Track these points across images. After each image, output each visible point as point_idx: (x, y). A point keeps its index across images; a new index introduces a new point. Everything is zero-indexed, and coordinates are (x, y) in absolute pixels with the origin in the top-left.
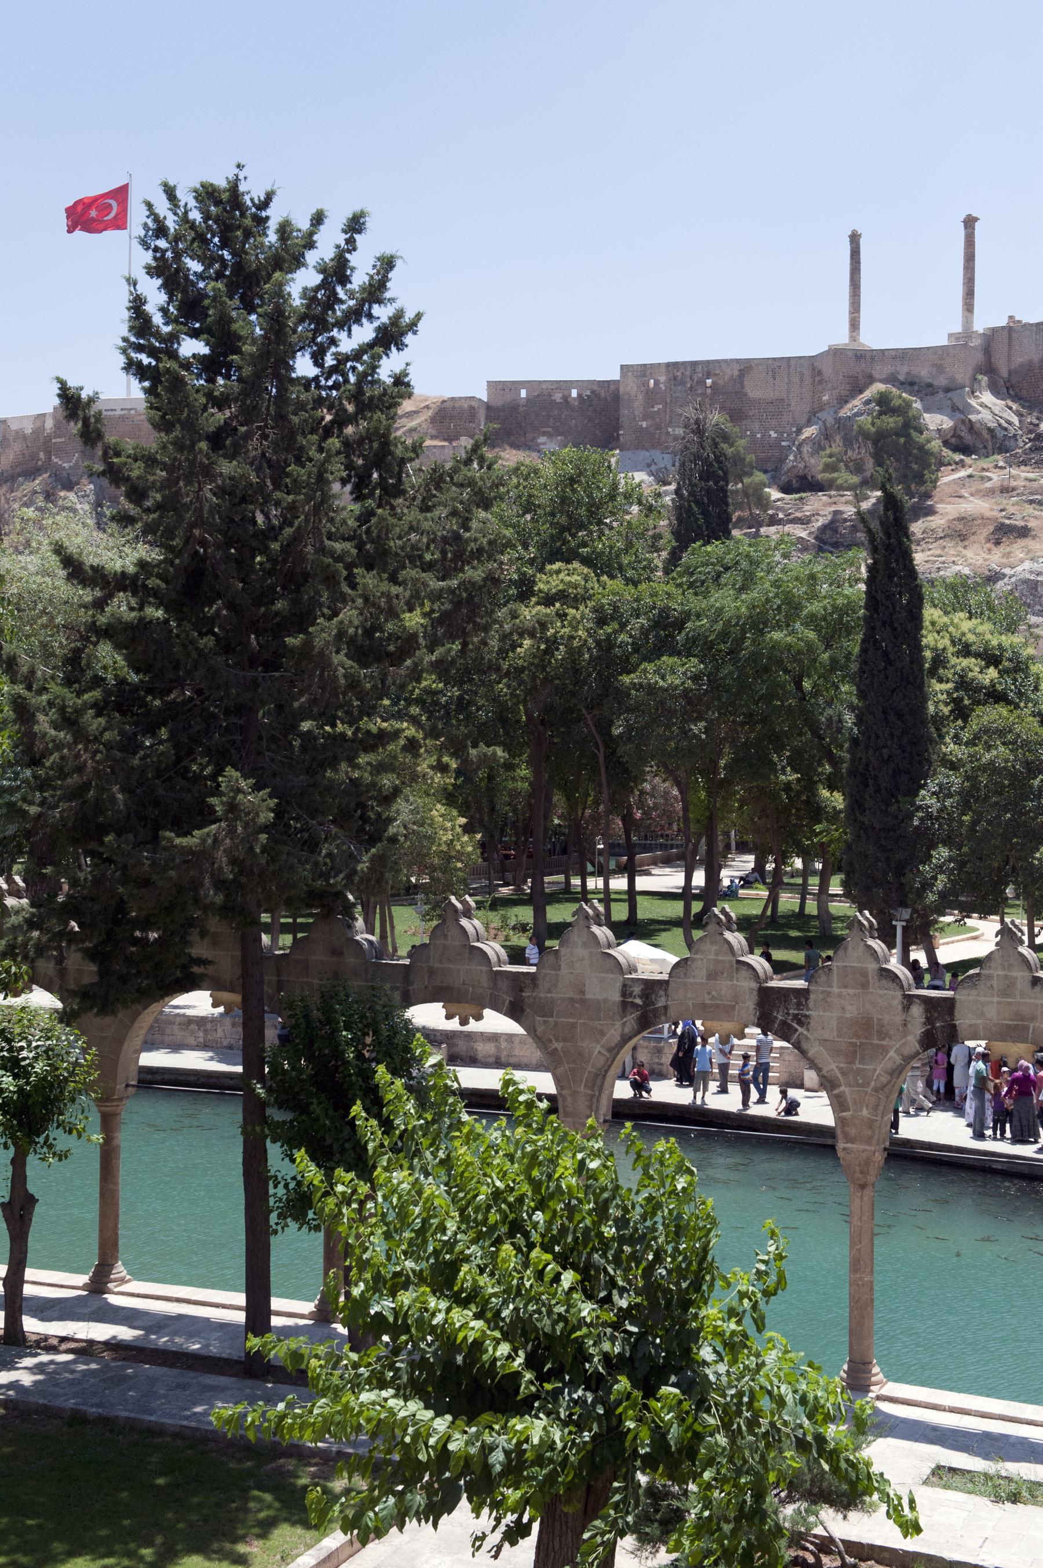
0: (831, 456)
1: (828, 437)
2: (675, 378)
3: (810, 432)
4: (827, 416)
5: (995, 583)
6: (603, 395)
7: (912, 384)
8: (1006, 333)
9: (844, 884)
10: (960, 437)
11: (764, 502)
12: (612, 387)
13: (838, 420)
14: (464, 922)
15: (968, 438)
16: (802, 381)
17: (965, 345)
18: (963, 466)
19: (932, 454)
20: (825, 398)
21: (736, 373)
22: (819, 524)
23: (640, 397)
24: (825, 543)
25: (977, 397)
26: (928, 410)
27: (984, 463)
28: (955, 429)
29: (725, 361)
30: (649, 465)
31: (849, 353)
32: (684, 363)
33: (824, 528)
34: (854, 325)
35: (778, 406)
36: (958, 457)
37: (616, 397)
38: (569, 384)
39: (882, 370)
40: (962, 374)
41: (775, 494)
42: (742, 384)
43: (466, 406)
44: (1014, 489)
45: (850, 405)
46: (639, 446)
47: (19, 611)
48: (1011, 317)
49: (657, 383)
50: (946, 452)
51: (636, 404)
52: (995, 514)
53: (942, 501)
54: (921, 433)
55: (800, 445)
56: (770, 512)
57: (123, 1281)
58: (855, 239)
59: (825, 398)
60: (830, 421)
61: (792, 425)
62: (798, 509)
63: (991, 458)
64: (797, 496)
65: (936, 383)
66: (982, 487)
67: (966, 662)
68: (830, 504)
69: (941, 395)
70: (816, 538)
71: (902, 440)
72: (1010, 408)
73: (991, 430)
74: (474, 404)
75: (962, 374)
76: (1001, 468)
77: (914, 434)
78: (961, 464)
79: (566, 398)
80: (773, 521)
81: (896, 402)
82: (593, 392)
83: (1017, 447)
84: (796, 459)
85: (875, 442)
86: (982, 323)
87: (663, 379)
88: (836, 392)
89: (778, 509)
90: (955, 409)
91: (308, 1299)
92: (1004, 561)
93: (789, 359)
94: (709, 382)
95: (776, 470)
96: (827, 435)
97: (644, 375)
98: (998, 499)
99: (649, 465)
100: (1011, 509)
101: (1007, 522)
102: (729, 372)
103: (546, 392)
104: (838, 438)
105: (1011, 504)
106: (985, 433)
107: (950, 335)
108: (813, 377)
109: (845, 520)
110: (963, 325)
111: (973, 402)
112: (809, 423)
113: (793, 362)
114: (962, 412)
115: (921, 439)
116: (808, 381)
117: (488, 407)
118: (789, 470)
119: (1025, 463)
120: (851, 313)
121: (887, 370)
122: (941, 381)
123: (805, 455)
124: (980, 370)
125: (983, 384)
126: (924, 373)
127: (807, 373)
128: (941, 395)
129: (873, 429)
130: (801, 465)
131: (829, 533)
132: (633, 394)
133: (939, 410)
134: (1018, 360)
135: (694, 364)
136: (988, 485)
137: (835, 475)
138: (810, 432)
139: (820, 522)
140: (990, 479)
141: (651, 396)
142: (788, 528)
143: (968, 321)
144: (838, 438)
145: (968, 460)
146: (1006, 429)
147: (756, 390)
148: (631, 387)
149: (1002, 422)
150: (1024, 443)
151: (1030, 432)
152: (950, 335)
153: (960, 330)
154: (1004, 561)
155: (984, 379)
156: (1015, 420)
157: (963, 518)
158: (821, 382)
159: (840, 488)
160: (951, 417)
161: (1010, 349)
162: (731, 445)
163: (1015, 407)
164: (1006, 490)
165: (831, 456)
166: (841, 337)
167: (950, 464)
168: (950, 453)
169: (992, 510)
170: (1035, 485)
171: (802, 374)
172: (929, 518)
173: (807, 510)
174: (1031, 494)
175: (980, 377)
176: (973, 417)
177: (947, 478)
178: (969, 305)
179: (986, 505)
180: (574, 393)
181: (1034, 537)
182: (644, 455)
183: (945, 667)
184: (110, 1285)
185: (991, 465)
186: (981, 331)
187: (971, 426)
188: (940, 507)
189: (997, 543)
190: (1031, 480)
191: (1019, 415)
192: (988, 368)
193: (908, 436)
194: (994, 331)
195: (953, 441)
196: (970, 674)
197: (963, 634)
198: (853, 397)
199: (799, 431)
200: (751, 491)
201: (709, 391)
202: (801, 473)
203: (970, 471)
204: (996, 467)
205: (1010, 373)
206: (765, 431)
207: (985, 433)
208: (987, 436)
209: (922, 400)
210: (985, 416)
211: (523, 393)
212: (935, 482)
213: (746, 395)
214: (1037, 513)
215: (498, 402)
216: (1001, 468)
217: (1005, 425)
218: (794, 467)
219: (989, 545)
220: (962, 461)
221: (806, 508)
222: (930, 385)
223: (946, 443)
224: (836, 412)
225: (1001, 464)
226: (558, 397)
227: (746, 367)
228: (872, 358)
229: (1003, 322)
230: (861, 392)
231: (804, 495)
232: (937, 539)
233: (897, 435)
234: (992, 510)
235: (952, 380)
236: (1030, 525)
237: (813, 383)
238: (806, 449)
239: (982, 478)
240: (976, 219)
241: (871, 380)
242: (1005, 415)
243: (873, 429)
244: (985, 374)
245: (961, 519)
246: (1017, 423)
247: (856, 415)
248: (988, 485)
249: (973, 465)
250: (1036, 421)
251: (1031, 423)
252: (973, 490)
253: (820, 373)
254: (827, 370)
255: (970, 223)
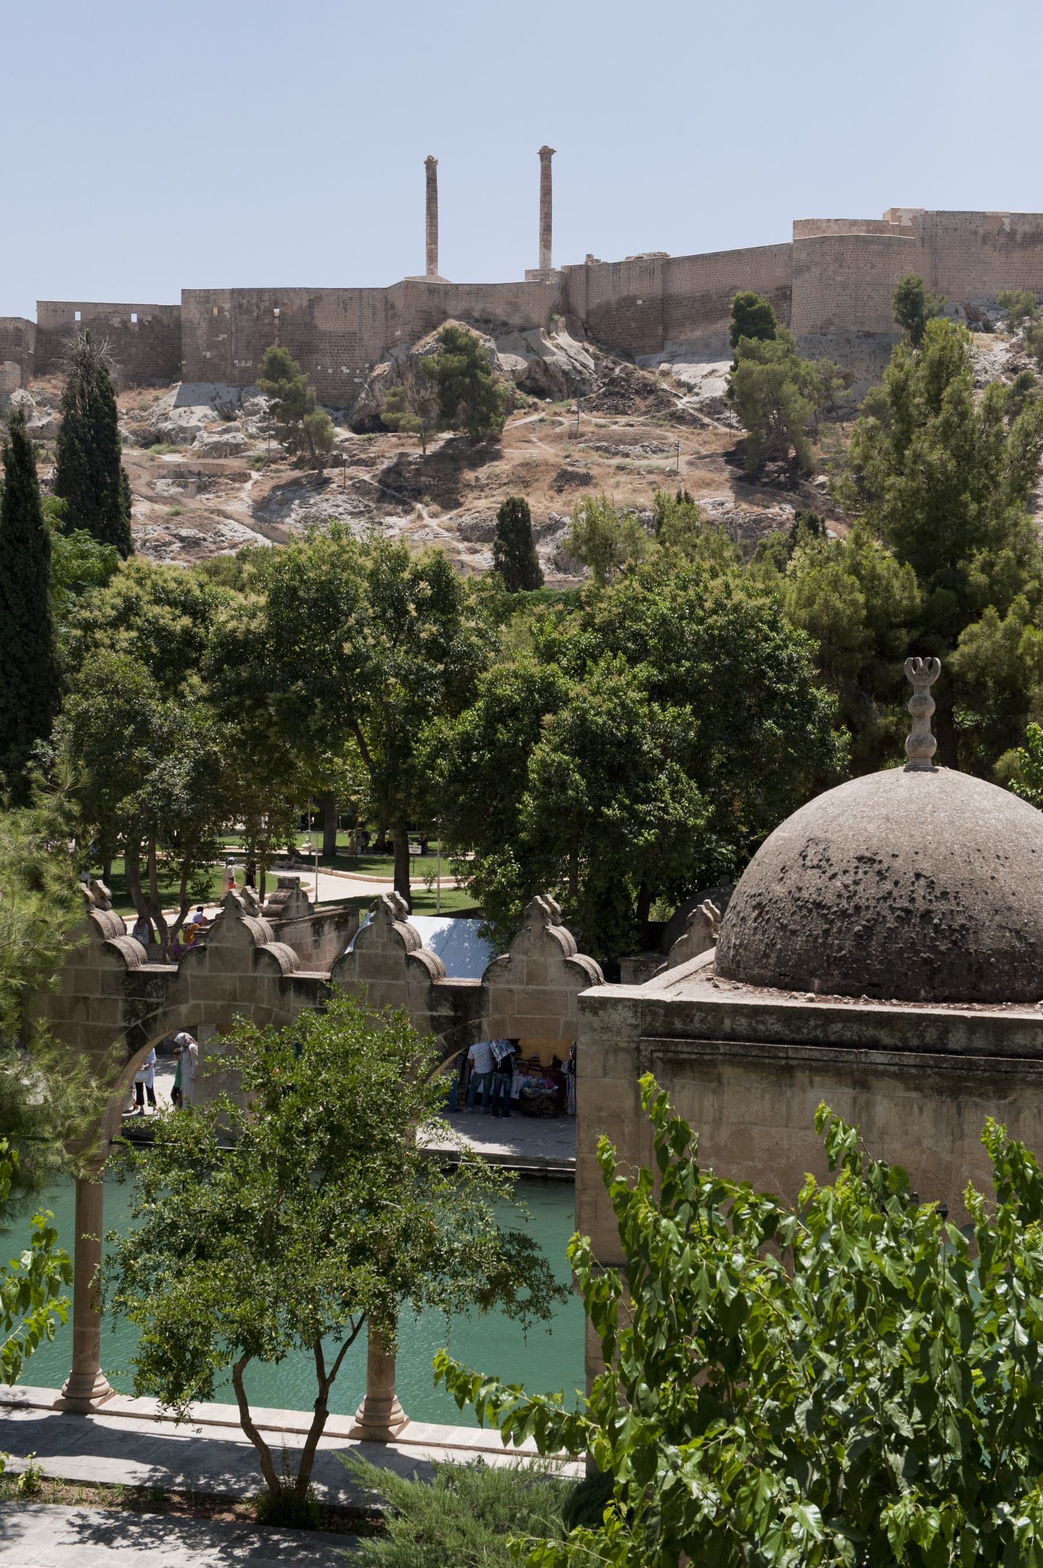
0: (394, 395)
1: (400, 375)
2: (240, 306)
3: (382, 368)
4: (399, 352)
5: (555, 532)
6: (166, 321)
7: (487, 321)
8: (583, 272)
9: (126, 854)
10: (535, 380)
11: (326, 443)
12: (176, 313)
13: (411, 358)
14: (247, 920)
15: (543, 381)
16: (374, 314)
17: (539, 284)
18: (536, 410)
19: (499, 396)
20: (398, 333)
21: (305, 303)
22: (384, 466)
23: (204, 325)
24: (388, 487)
25: (554, 338)
26: (502, 350)
27: (558, 407)
28: (529, 370)
29: (294, 290)
30: (213, 399)
31: (422, 287)
32: (250, 290)
33: (388, 471)
34: (432, 257)
35: (349, 341)
36: (531, 400)
37: (179, 324)
38: (129, 308)
39: (455, 306)
40: (537, 314)
41: (342, 433)
42: (311, 314)
43: (11, 327)
44: (582, 435)
45: (422, 342)
46: (202, 378)
47: (740, 576)
48: (589, 256)
49: (221, 310)
50: (520, 394)
51: (199, 332)
52: (560, 460)
53: (509, 446)
54: (489, 374)
55: (372, 382)
56: (335, 453)
57: (106, 1395)
58: (431, 165)
59: (398, 333)
60: (402, 358)
61: (365, 361)
62: (365, 451)
63: (566, 402)
64: (366, 436)
65: (511, 322)
66: (550, 432)
67: (157, 609)
68: (397, 446)
69: (516, 334)
70: (380, 482)
71: (467, 380)
72: (587, 351)
73: (565, 373)
74: (19, 325)
75: (537, 314)
76: (573, 412)
77: (480, 374)
78: (535, 407)
79: (125, 323)
80: (338, 462)
81: (462, 341)
82: (154, 317)
83: (592, 391)
84: (367, 398)
85: (441, 383)
86: (560, 261)
87: (227, 306)
88: (408, 327)
89: (344, 449)
90: (530, 349)
91: (56, 1386)
92: (565, 509)
93: (361, 290)
94: (277, 311)
95: (348, 408)
96: (399, 373)
97: (208, 302)
98: (565, 445)
99: (213, 399)
100: (576, 456)
101: (570, 469)
102: (297, 301)
103: (102, 316)
104: (410, 376)
105: (577, 451)
106: (559, 375)
107: (527, 272)
108: (386, 310)
109: (410, 463)
110: (541, 262)
111: (548, 343)
112: (382, 359)
113: (365, 294)
114: (537, 354)
115: (487, 381)
116: (381, 314)
117: (39, 330)
118: (361, 409)
119: (597, 408)
120: (428, 244)
121: (461, 306)
122: (516, 320)
123: (377, 393)
124: (556, 309)
125: (560, 324)
126: (499, 311)
127: (380, 305)
128: (516, 334)
129: (437, 368)
130: (373, 404)
131: (392, 476)
132: (195, 321)
133: (514, 350)
134: (596, 301)
135: (261, 292)
136: (558, 430)
137: (399, 415)
138: (382, 368)
139: (386, 464)
140: (561, 424)
141: (215, 324)
142: (351, 471)
143: (545, 259)
144: (410, 376)
145: (541, 404)
146: (580, 372)
147: (326, 322)
148: (193, 314)
149: (577, 364)
150: (598, 388)
151: (605, 376)
152: (527, 272)
153: (537, 267)
154: (565, 509)
155: (561, 320)
156: (591, 363)
157: (527, 464)
158: (394, 316)
159: (404, 429)
160: (526, 358)
161: (587, 289)
162: (290, 381)
163: (591, 349)
164: (574, 436)
165: (394, 395)
166: (417, 269)
167: (523, 407)
168: (524, 396)
169: (557, 456)
170: (603, 431)
171: (374, 307)
172: (495, 463)
173: (373, 451)
174: (599, 440)
175: (556, 317)
176: (548, 359)
177: (515, 423)
178: (546, 243)
179: (552, 451)
180: (134, 318)
181: (596, 485)
182: (208, 388)
183: (137, 614)
184: (94, 1402)
185: (564, 410)
186: (559, 269)
187: (546, 368)
188: (507, 452)
189: (560, 491)
190: (601, 426)
191: (595, 357)
192: (566, 308)
193: (474, 376)
194: (572, 270)
195: (528, 383)
196: (161, 621)
197: (165, 581)
198: (426, 333)
199: (372, 368)
200: (312, 429)
201: (277, 321)
202: (373, 412)
203: (543, 415)
204: (569, 411)
205: (588, 314)
206: (337, 366)
207: (559, 375)
208: (562, 379)
209: (496, 339)
210: (560, 358)
211: (78, 316)
212: (501, 425)
213: (316, 327)
214: (601, 460)
215: (50, 324)
216: (573, 412)
217: (580, 368)
218: (365, 405)
219: (551, 493)
220: (535, 404)
221: (373, 449)
222: (505, 324)
223: (520, 385)
224: (408, 349)
225: (574, 408)
226: (116, 321)
227: (316, 297)
228: (446, 293)
229: (581, 261)
230: (435, 328)
231: (372, 435)
232: (501, 485)
233: (464, 375)
234: (557, 456)
235: (527, 319)
236: (591, 472)
237: (386, 316)
238: (377, 386)
239: (553, 423)
240: (552, 152)
241: (445, 316)
242: (580, 358)
243: (437, 368)
244: (561, 314)
245: (525, 465)
246: (592, 367)
247: (428, 352)
248: (558, 430)
249: (547, 408)
250: (611, 365)
251: (606, 367)
252: (542, 434)
253: (393, 307)
254: (400, 304)
255: (546, 154)
